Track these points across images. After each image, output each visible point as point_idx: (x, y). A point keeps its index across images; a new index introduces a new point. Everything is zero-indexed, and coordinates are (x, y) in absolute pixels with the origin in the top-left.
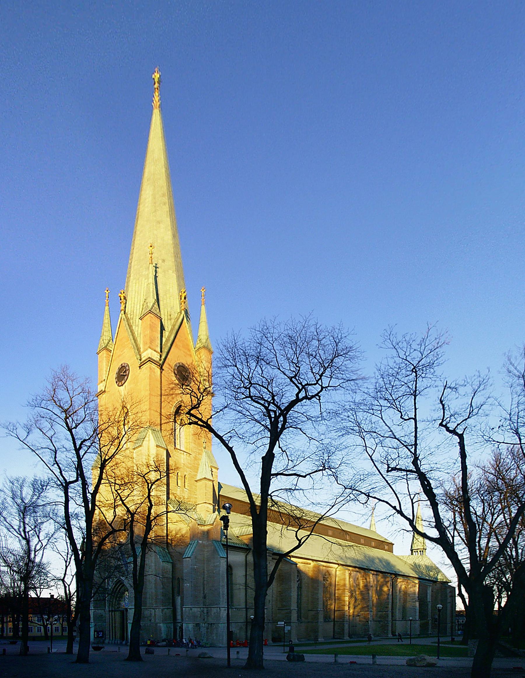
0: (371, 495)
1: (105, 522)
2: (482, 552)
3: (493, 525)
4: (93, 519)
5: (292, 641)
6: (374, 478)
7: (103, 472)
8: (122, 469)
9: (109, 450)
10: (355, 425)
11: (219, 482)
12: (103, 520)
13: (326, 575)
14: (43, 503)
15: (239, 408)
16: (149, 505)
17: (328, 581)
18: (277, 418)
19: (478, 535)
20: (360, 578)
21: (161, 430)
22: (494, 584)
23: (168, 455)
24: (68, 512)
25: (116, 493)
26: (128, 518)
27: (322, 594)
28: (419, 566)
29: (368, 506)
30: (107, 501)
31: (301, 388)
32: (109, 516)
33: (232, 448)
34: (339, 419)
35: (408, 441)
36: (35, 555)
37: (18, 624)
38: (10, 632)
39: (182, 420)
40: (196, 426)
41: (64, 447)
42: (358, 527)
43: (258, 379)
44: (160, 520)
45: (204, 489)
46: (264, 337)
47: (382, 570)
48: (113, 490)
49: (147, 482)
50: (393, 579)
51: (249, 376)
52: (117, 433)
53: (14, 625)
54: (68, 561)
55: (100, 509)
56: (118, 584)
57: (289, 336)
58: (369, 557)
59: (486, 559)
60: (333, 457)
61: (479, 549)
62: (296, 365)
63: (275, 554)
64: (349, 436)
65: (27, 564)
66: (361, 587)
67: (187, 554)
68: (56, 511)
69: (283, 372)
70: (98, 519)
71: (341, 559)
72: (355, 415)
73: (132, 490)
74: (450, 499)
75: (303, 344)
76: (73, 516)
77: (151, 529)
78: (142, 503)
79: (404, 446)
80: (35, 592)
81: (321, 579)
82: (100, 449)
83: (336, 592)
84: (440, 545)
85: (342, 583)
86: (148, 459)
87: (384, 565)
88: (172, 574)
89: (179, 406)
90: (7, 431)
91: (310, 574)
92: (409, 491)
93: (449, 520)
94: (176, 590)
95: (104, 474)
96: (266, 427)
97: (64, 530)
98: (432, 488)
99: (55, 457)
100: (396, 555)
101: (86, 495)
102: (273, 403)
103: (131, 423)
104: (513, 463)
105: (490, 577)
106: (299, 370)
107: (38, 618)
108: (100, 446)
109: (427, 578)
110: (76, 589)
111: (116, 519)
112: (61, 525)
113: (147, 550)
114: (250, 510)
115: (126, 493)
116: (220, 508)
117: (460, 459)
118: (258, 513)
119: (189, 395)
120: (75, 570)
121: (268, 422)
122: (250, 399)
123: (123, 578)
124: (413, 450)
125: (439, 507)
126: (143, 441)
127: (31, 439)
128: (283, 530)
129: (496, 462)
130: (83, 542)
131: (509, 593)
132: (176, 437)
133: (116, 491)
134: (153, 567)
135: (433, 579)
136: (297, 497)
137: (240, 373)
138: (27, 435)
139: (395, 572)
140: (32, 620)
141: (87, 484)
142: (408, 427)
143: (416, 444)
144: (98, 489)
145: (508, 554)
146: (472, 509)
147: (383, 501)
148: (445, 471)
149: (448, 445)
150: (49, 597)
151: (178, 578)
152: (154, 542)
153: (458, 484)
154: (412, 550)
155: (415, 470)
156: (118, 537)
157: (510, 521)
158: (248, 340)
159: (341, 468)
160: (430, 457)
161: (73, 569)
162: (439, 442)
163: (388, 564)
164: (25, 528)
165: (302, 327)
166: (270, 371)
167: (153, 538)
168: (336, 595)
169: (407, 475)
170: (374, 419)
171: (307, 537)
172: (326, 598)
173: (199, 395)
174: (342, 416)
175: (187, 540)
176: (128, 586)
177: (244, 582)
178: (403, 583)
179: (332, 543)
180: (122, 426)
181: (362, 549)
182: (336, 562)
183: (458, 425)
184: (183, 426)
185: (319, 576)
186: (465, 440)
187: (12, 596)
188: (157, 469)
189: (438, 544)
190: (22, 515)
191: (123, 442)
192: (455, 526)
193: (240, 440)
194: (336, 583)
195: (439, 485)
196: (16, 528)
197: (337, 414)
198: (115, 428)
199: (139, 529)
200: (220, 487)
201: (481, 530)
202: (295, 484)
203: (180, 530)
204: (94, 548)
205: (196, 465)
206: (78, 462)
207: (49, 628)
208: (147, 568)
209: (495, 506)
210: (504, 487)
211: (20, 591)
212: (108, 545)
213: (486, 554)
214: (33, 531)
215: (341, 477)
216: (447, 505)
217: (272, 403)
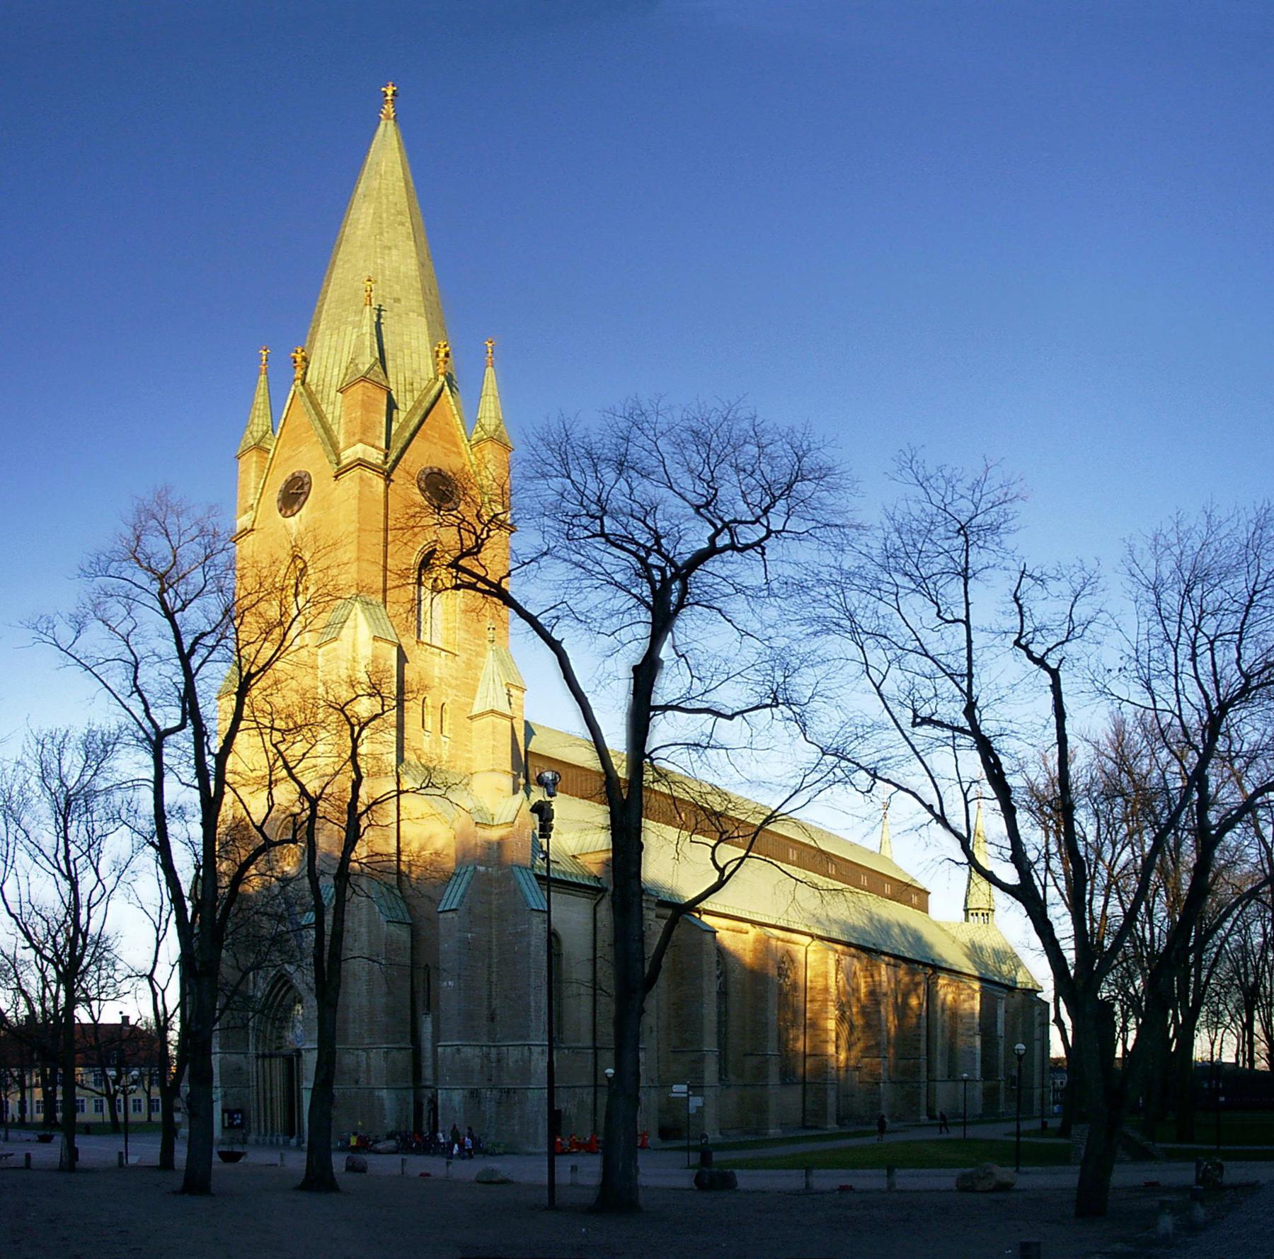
0: (879, 775)
1: (248, 825)
2: (1096, 925)
3: (1113, 870)
4: (220, 819)
5: (707, 1137)
6: (885, 735)
7: (244, 703)
8: (289, 694)
9: (258, 652)
10: (842, 616)
11: (526, 722)
12: (243, 820)
13: (784, 963)
14: (104, 785)
15: (576, 558)
16: (354, 776)
17: (789, 977)
18: (666, 583)
19: (1089, 888)
20: (860, 974)
21: (385, 601)
22: (1115, 998)
23: (402, 658)
24: (163, 806)
25: (275, 751)
26: (303, 810)
27: (776, 1012)
28: (981, 949)
29: (873, 798)
30: (252, 771)
31: (719, 526)
32: (258, 809)
33: (561, 642)
34: (807, 599)
35: (955, 666)
36: (89, 918)
37: (54, 1091)
38: (38, 1112)
39: (435, 580)
40: (473, 593)
41: (155, 654)
42: (852, 845)
43: (621, 504)
44: (381, 812)
45: (491, 737)
46: (635, 428)
47: (906, 955)
48: (268, 745)
49: (350, 723)
50: (928, 979)
51: (599, 497)
52: (278, 613)
53: (46, 1094)
54: (163, 926)
55: (235, 792)
56: (280, 985)
57: (693, 431)
58: (879, 921)
59: (1102, 942)
60: (795, 680)
61: (1090, 919)
62: (708, 484)
63: (663, 904)
64: (829, 638)
65: (72, 941)
66: (862, 995)
67: (449, 903)
68: (134, 804)
69: (680, 494)
70: (230, 817)
71: (818, 921)
72: (841, 596)
73: (313, 742)
74: (1039, 802)
75: (724, 448)
76: (173, 813)
77: (360, 837)
78: (337, 773)
79: (947, 674)
80: (88, 1009)
81: (773, 972)
82: (239, 651)
83: (808, 1006)
84: (1021, 901)
85: (820, 984)
86: (353, 670)
87: (909, 942)
88: (412, 953)
89: (430, 552)
90: (34, 633)
91: (748, 957)
92: (958, 774)
93: (1037, 848)
94: (421, 996)
95: (245, 707)
96: (641, 600)
97: (152, 850)
98: (1004, 774)
99: (135, 678)
100: (934, 919)
101: (204, 759)
102: (659, 552)
103: (312, 590)
104: (1145, 743)
105: (1110, 985)
106: (715, 495)
107: (95, 1075)
108: (237, 644)
109: (996, 979)
110: (178, 1000)
111: (273, 814)
112: (146, 838)
113: (349, 892)
114: (604, 789)
115: (298, 749)
116: (531, 781)
117: (1053, 719)
118: (625, 797)
119: (454, 529)
120: (178, 951)
121: (646, 590)
122: (603, 540)
123: (290, 968)
124: (964, 685)
125: (1018, 816)
126: (341, 628)
127: (83, 646)
128: (680, 842)
129: (1117, 736)
130: (197, 876)
131: (1140, 1020)
132: (423, 616)
133: (275, 746)
134: (364, 938)
135: (1007, 982)
136: (713, 764)
137: (578, 490)
138: (76, 638)
139: (933, 960)
140: (82, 1080)
141: (205, 733)
142: (954, 637)
143: (970, 675)
144: (232, 744)
145: (1138, 936)
146: (1077, 828)
147: (907, 790)
148: (1027, 741)
149: (1031, 687)
150: (119, 1021)
151: (427, 965)
152: (366, 870)
153: (1052, 771)
154: (966, 911)
155: (969, 728)
156: (277, 861)
157: (1142, 860)
158: (597, 431)
159: (813, 705)
160: (998, 706)
161: (172, 947)
162: (1015, 678)
163: (918, 940)
164: (67, 852)
165: (721, 420)
166: (647, 490)
167: (364, 861)
168: (808, 1015)
169: (954, 738)
170: (883, 609)
171: (738, 862)
172: (785, 1021)
173: (479, 528)
174: (812, 593)
175: (450, 865)
176: (301, 987)
177: (590, 976)
178: (950, 990)
179: (797, 880)
180: (291, 599)
181: (863, 899)
182: (807, 931)
183: (1049, 650)
184: (439, 592)
185: (767, 965)
186: (1062, 682)
187: (40, 1021)
188: (375, 691)
189: (1017, 899)
190: (61, 820)
191: (292, 633)
192: (1047, 863)
193: (580, 626)
194: (808, 984)
195: (1017, 769)
196: (50, 853)
197: (802, 588)
198: (274, 603)
199: (329, 838)
200: (529, 731)
201: (1093, 878)
202: (708, 734)
203: (430, 837)
204: (220, 891)
205: (472, 682)
206: (186, 684)
207: (119, 1101)
208: (348, 940)
209: (1117, 826)
210: (1130, 790)
211: (56, 1011)
212: (253, 885)
213: (1102, 930)
214: (84, 857)
215: (815, 727)
216: (1033, 813)
217: (654, 551)
